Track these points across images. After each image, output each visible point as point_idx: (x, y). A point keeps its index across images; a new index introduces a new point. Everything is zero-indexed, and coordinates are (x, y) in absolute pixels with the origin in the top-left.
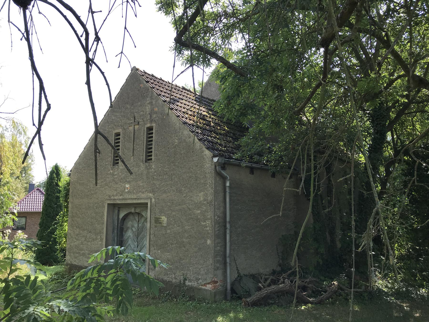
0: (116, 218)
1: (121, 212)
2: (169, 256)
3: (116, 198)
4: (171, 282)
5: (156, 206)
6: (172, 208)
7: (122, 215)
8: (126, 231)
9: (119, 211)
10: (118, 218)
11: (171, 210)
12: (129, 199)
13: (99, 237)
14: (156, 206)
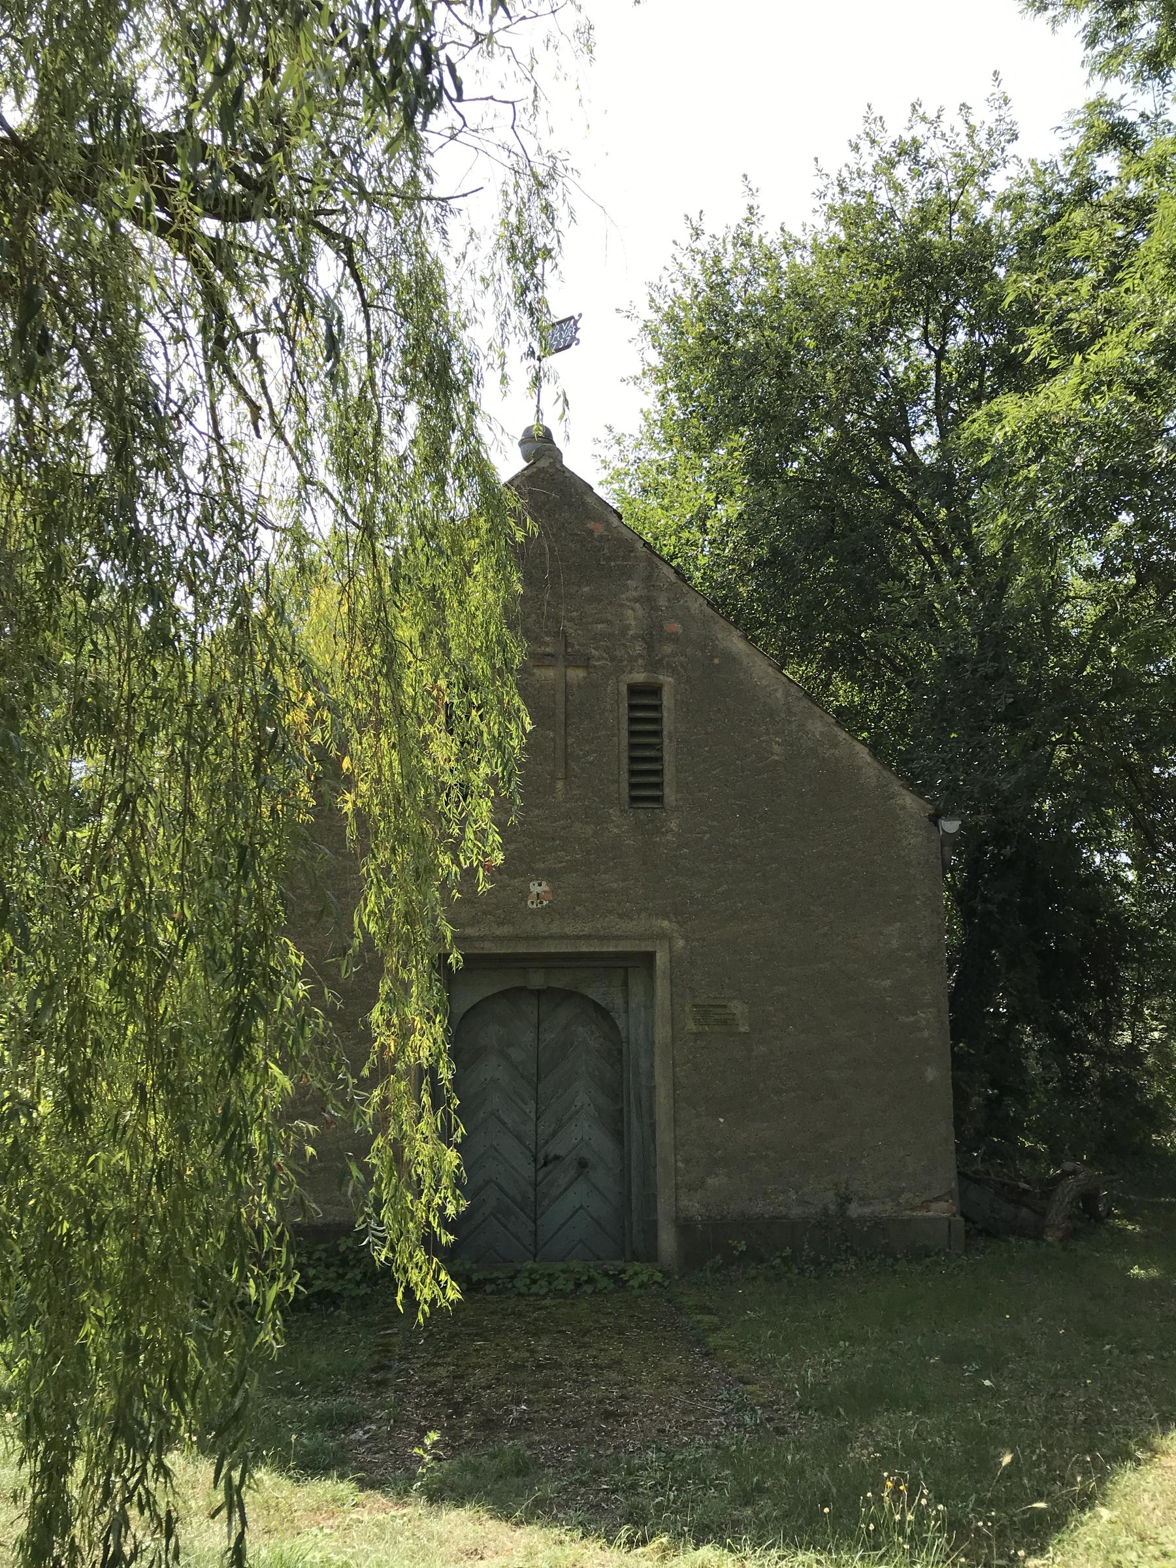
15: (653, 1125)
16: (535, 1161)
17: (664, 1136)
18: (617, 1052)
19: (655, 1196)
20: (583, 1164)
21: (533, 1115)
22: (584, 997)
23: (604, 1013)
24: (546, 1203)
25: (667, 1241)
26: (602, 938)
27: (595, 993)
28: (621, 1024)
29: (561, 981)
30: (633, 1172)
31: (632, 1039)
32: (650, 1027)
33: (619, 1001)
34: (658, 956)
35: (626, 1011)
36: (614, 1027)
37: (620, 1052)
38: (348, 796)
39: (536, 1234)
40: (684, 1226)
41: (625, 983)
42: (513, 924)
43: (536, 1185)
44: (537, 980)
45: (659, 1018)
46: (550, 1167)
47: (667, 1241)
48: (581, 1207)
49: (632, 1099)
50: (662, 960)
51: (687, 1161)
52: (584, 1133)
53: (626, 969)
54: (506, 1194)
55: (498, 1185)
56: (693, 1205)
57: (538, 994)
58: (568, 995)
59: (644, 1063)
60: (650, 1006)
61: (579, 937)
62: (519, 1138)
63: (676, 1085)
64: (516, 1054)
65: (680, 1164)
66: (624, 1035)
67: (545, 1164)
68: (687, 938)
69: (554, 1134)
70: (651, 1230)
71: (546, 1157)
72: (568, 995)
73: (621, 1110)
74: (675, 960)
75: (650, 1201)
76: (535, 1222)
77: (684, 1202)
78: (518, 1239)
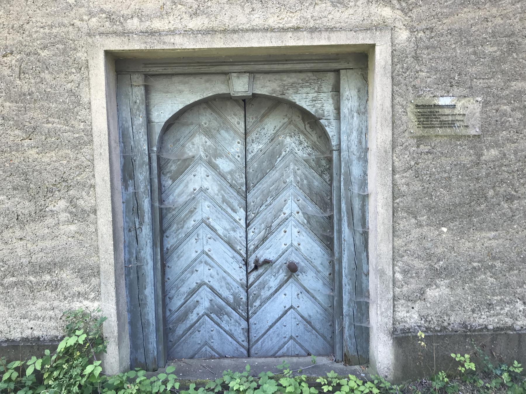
0: (140, 120)
1: (156, 98)
2: (494, 243)
3: (157, 24)
4: (511, 328)
5: (416, 58)
6: (506, 67)
7: (163, 112)
8: (181, 172)
9: (147, 90)
10: (149, 122)
11: (503, 72)
12: (253, 30)
13: (62, 204)
14: (416, 58)
15: (365, 235)
16: (246, 264)
17: (380, 247)
18: (326, 160)
19: (367, 305)
20: (292, 269)
21: (243, 222)
22: (293, 106)
23: (311, 121)
24: (257, 303)
25: (383, 353)
26: (313, 30)
27: (303, 99)
28: (331, 131)
29: (266, 87)
30: (345, 280)
31: (344, 146)
32: (364, 133)
33: (329, 107)
34: (377, 49)
35: (338, 117)
36: (324, 135)
37: (330, 160)
38: (419, 334)
39: (248, 331)
40: (402, 338)
41: (337, 90)
42: (208, 15)
43: (247, 287)
44: (240, 86)
45: (372, 125)
46: (260, 271)
47: (383, 353)
48: (291, 307)
49: (343, 205)
50: (382, 57)
51: (405, 272)
52: (293, 239)
53: (337, 72)
54: (220, 296)
55: (212, 288)
56: (411, 317)
57: (246, 103)
58: (276, 104)
59: (356, 171)
60: (363, 111)
61: (284, 30)
62: (230, 244)
63: (395, 194)
64: (224, 165)
65: (399, 276)
66: (334, 143)
67: (256, 268)
68: (412, 30)
69: (264, 239)
70: (363, 335)
71: (257, 261)
72: (276, 104)
73: (331, 218)
74: (397, 56)
75: (362, 309)
76: (247, 320)
77: (401, 314)
78: (232, 336)
